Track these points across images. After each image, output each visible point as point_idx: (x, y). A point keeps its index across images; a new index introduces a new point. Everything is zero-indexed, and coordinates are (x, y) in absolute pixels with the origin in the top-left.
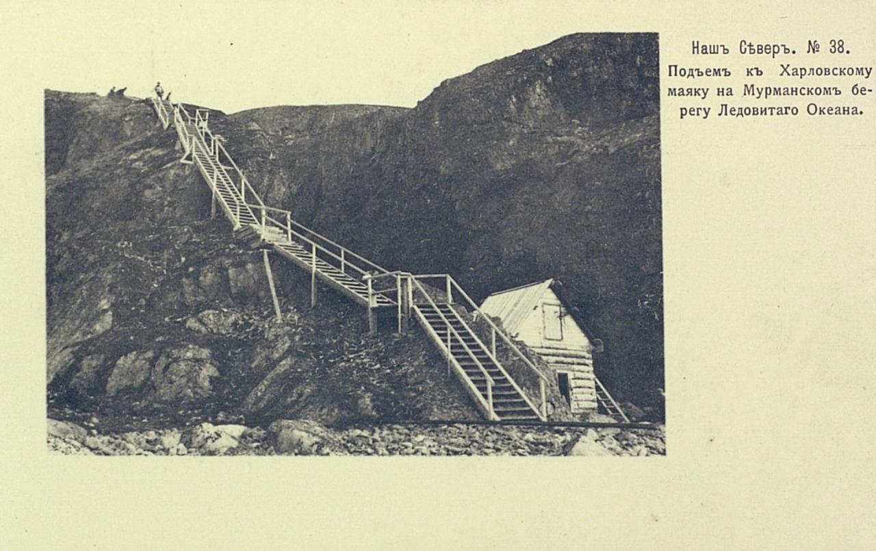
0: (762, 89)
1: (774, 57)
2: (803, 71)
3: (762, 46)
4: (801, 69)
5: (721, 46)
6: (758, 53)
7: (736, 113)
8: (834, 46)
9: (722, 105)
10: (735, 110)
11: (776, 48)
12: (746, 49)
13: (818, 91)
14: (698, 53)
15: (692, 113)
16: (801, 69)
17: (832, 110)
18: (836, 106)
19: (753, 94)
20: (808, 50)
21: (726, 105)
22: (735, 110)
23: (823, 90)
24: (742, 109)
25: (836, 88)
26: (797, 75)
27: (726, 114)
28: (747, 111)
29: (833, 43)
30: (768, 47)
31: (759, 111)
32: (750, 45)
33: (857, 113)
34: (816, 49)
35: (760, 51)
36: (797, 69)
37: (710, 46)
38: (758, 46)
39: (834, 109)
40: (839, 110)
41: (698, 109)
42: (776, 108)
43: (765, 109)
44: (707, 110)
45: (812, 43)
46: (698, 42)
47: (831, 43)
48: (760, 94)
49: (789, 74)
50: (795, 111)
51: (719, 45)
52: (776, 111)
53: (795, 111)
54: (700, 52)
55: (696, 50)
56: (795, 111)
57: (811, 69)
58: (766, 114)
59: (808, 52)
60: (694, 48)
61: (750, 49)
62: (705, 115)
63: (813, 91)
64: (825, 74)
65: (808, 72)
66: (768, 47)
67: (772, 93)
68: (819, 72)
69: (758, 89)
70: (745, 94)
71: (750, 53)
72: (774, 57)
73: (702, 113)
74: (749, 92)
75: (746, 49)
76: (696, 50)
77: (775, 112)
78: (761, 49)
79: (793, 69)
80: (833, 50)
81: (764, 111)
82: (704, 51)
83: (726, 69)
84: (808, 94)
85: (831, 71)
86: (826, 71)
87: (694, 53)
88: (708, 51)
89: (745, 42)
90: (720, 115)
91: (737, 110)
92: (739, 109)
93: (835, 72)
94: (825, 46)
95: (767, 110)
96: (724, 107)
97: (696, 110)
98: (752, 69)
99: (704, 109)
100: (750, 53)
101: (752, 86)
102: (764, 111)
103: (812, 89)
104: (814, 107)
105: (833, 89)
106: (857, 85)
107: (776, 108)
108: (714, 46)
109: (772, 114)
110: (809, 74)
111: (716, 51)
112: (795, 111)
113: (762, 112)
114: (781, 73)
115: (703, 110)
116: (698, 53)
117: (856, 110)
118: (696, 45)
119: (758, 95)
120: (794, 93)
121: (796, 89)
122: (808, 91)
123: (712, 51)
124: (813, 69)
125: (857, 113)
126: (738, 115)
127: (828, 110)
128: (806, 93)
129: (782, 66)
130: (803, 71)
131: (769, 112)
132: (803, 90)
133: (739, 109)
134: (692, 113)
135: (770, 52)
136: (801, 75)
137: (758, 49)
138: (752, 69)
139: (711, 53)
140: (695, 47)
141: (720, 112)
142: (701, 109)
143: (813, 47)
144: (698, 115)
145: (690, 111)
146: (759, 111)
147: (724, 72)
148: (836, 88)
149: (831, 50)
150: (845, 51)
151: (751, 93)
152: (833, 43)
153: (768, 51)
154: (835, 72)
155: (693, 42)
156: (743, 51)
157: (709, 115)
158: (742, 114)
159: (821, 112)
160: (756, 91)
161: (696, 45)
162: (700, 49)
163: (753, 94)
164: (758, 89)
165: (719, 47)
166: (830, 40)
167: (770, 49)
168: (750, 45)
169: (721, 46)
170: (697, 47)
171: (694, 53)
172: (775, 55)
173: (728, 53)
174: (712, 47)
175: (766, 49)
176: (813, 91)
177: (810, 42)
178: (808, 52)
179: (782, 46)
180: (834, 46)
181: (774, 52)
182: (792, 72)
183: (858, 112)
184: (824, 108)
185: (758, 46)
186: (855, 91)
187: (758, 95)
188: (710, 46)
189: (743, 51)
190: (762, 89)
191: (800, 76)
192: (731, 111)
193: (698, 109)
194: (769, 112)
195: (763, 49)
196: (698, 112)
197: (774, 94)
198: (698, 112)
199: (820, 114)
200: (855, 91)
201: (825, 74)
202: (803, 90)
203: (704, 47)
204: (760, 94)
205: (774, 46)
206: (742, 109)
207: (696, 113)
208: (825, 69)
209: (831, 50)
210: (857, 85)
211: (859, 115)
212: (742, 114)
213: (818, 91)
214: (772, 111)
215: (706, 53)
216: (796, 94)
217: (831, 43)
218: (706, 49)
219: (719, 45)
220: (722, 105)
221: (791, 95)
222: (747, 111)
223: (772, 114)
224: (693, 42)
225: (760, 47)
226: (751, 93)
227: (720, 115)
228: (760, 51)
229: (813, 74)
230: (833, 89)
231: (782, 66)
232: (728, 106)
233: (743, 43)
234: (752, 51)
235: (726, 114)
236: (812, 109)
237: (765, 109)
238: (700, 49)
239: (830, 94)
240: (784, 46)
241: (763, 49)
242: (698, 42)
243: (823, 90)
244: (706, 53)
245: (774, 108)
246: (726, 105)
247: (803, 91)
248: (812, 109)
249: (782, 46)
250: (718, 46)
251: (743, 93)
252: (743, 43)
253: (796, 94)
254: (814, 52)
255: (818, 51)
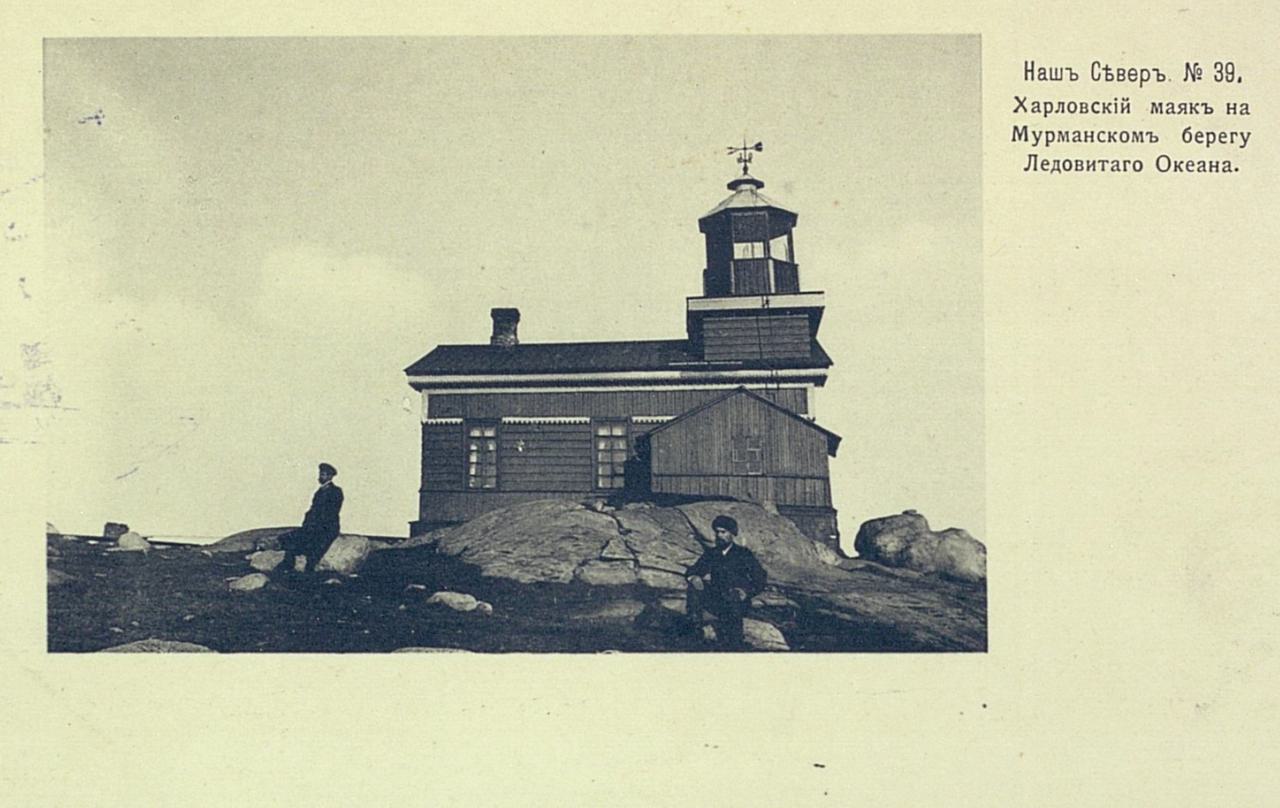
0: (1041, 132)
1: (1141, 86)
2: (1048, 106)
3: (1124, 71)
4: (1045, 104)
5: (1067, 69)
6: (1118, 80)
7: (1050, 167)
8: (1220, 72)
9: (1030, 156)
10: (1048, 164)
11: (1145, 73)
12: (1100, 75)
13: (1124, 137)
14: (1033, 78)
15: (1199, 139)
16: (1045, 104)
17: (1193, 165)
18: (1225, 160)
19: (1026, 140)
20: (1184, 77)
21: (1036, 156)
22: (1048, 164)
23: (1131, 135)
24: (1058, 161)
25: (1151, 133)
26: (1039, 111)
27: (1035, 169)
28: (1067, 165)
29: (1219, 67)
30: (1133, 72)
31: (1085, 165)
32: (1107, 69)
33: (1230, 170)
34: (1197, 76)
35: (1121, 78)
36: (1038, 103)
37: (1051, 70)
38: (1119, 70)
39: (1195, 163)
40: (1204, 166)
41: (1232, 134)
42: (1110, 161)
43: (1094, 162)
44: (1245, 136)
45: (1192, 66)
46: (1033, 63)
47: (1215, 67)
48: (1037, 140)
49: (1025, 110)
50: (1138, 166)
51: (1064, 68)
52: (1111, 165)
53: (1139, 166)
54: (1036, 76)
55: (1029, 74)
56: (1138, 166)
57: (1059, 103)
58: (1094, 170)
59: (1185, 80)
60: (1027, 71)
61: (1107, 74)
62: (1243, 144)
63: (1117, 137)
64: (1081, 112)
65: (1056, 107)
66: (1133, 72)
67: (1056, 138)
68: (1072, 108)
69: (1034, 133)
70: (1014, 140)
71: (1107, 80)
72: (1141, 86)
73: (1238, 140)
74: (1020, 136)
75: (1100, 75)
76: (1029, 74)
77: (1108, 166)
78: (1123, 75)
79: (1033, 104)
80: (1219, 78)
81: (1092, 166)
82: (1042, 77)
83: (1206, 104)
84: (1110, 141)
85: (1089, 108)
86: (1082, 108)
87: (1026, 78)
88: (1048, 76)
89: (1098, 63)
90: (1026, 169)
91: (1052, 163)
92: (1055, 161)
93: (1096, 108)
94: (1209, 72)
95: (1097, 164)
96: (1033, 158)
97: (1229, 136)
98: (1197, 104)
99: (1242, 134)
100: (1107, 80)
101: (1025, 128)
102: (1092, 166)
103: (1115, 133)
104: (1165, 159)
105: (1147, 133)
106: (1189, 128)
107: (1110, 161)
108: (1056, 70)
109: (1103, 169)
110: (1057, 112)
111: (1059, 77)
112: (1139, 166)
113: (1088, 168)
114: (1014, 108)
115: (1239, 136)
116: (1033, 78)
117: (1229, 166)
118: (1029, 67)
119: (1034, 142)
120: (1089, 139)
121: (1092, 133)
122: (1110, 137)
123: (1054, 77)
124: (1063, 103)
125: (1230, 170)
126: (1053, 170)
127: (1187, 165)
128: (1107, 139)
129: (1017, 98)
130: (1048, 106)
131: (1099, 166)
132: (1101, 134)
133: (1055, 161)
134: (1199, 139)
135: (1136, 79)
136: (1046, 112)
137: (1119, 75)
138: (1197, 104)
139: (1051, 79)
140: (1029, 71)
141: (1026, 166)
142: (1236, 134)
143: (1193, 73)
144: (1232, 142)
145: (1220, 137)
146: (1085, 165)
147: (1204, 107)
148: (1151, 133)
149: (1216, 77)
150: (1236, 79)
151: (1023, 137)
152: (1219, 67)
153: (1133, 78)
154: (1096, 108)
155: (1026, 63)
156: (1096, 77)
157: (1248, 142)
158: (1059, 170)
159: (1177, 167)
160: (1030, 135)
161: (1029, 67)
162: (1036, 73)
163: (1026, 140)
164: (1034, 133)
165: (1064, 71)
166: (1214, 62)
167: (1136, 74)
168: (1107, 69)
169: (1067, 69)
170: (1032, 71)
171: (1026, 78)
172: (1144, 83)
173: (1163, 80)
174: (1054, 71)
175: (1129, 75)
176: (1117, 137)
177: (1188, 65)
178: (1185, 80)
179: (1154, 70)
180: (1220, 72)
181: (1142, 80)
182: (1032, 107)
183: (1232, 168)
184: (1182, 162)
185: (1119, 70)
186: (1187, 137)
187: (1034, 142)
188: (1051, 70)
189: (1096, 77)
190: (1041, 132)
191: (1043, 113)
192: (1042, 164)
193: (1232, 134)
194: (1099, 166)
195: (1126, 75)
196: (1232, 138)
197: (1133, 141)
198: (1232, 138)
199: (1176, 170)
200: (1187, 137)
201: (1081, 112)
202: (1101, 134)
203: (1042, 71)
204: (1037, 140)
205: (1142, 71)
206: (1058, 161)
207: (1228, 139)
208: (1081, 104)
209: (1216, 77)
210: (1189, 128)
211: (1234, 172)
212: (1059, 170)
213: (1124, 137)
214: (1103, 166)
215: (1045, 78)
216: (1092, 141)
217: (1215, 67)
218: (1044, 73)
219: (1064, 68)
220: (1030, 156)
221: (1083, 143)
222: (1067, 165)
223: (1103, 169)
224: (1026, 63)
225: (1121, 72)
226: (1023, 137)
227: (1026, 169)
228: (1121, 78)
229: (1063, 111)
230: (1147, 133)
231: (1017, 98)
232: (1038, 158)
233: (1096, 65)
234: (1110, 77)
235: (1035, 169)
236: (1163, 164)
237: (1094, 162)
238: (1036, 73)
239: (1142, 141)
240: (1157, 70)
241: (1126, 75)
242: (1033, 63)
243: (1131, 135)
244: (1045, 78)
245: (1107, 161)
246: (1036, 156)
247: (1102, 137)
248: (1163, 164)
249: (1154, 70)
250: (1062, 70)
251: (1011, 137)
252: (1096, 65)
253: (1092, 141)
254: (1194, 80)
255: (1199, 78)
